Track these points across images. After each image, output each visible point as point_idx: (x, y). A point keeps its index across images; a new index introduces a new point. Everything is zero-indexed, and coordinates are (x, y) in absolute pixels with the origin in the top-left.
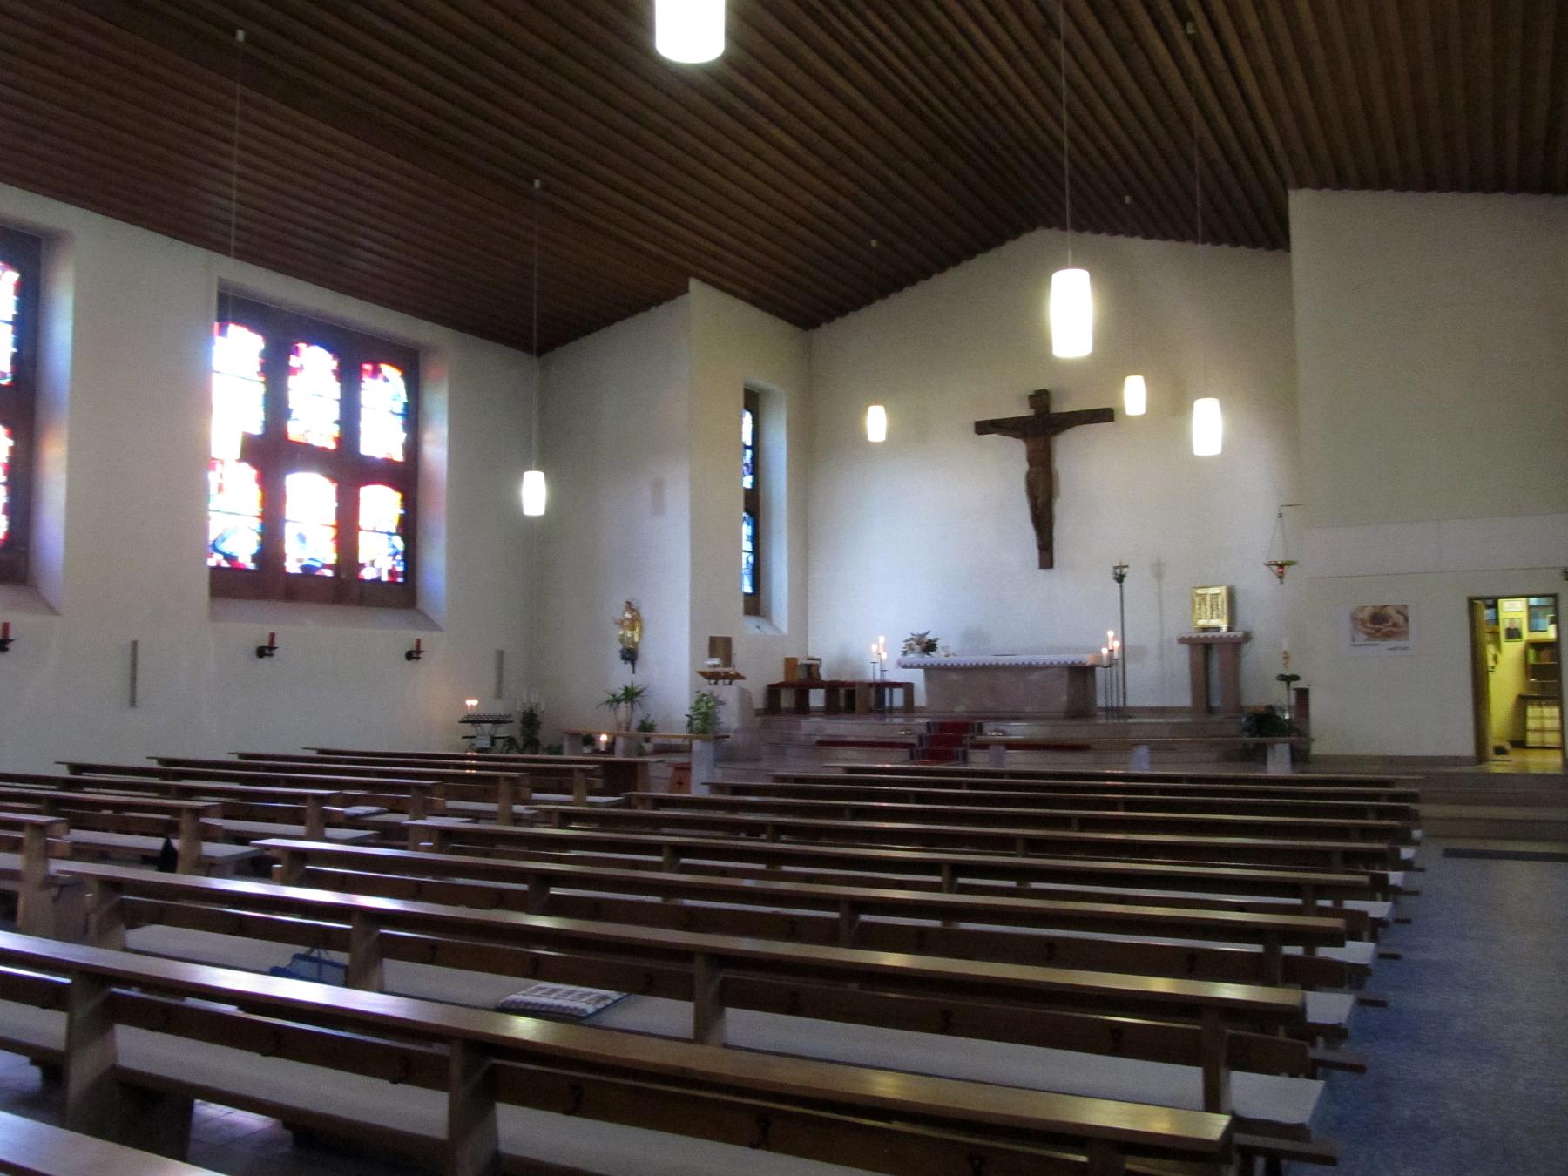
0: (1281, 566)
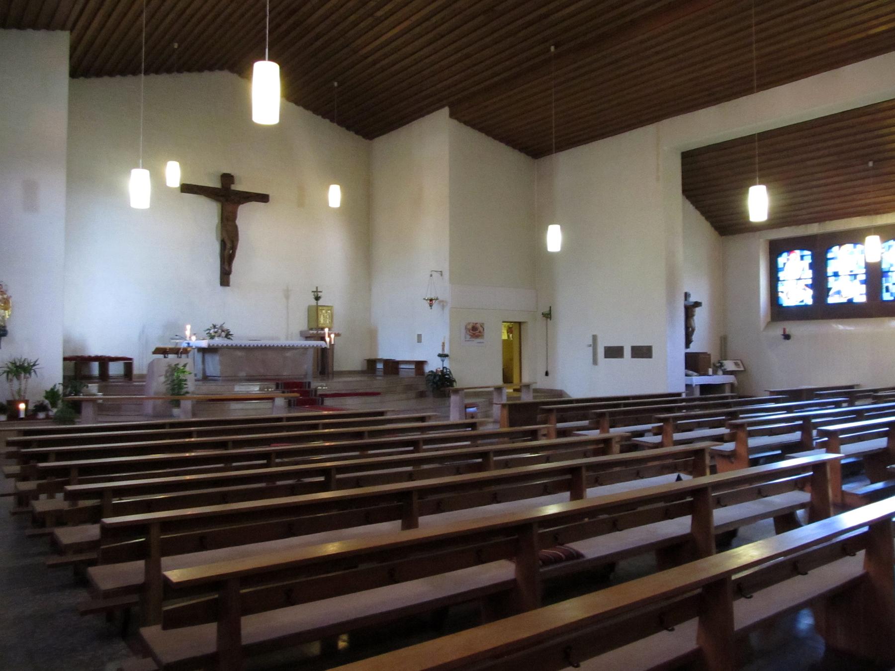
0: (431, 300)
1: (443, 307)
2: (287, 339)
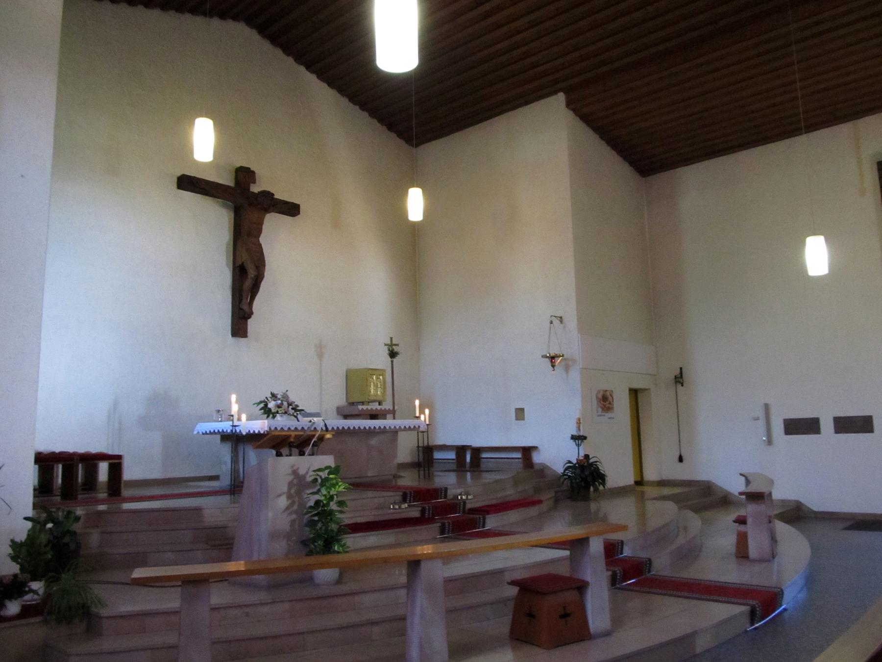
0: (552, 358)
1: (567, 368)
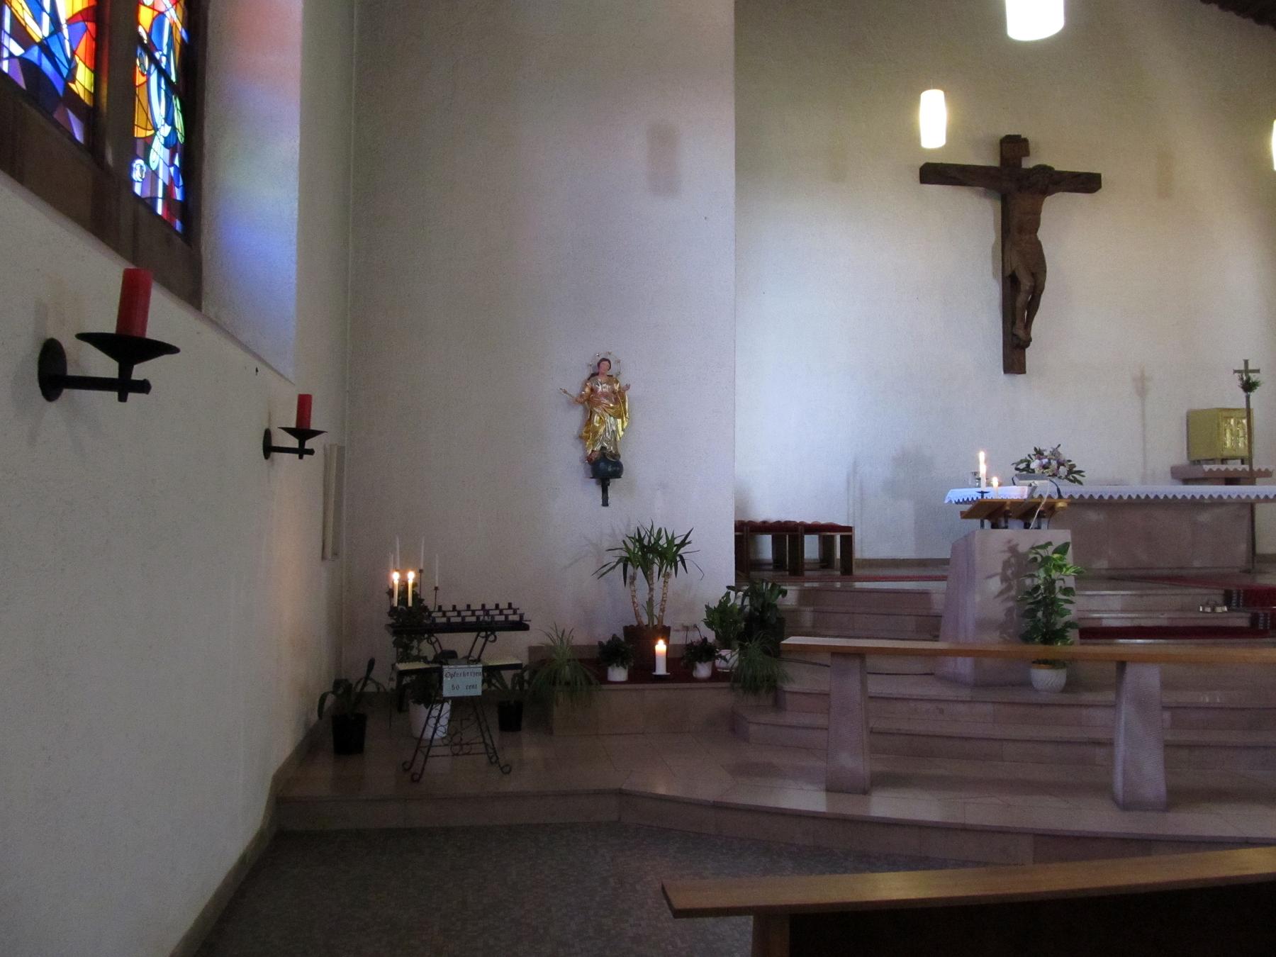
2: (1144, 481)
